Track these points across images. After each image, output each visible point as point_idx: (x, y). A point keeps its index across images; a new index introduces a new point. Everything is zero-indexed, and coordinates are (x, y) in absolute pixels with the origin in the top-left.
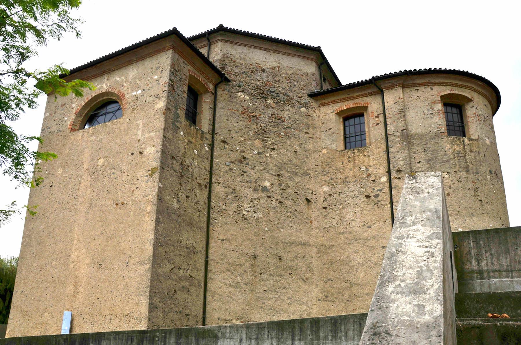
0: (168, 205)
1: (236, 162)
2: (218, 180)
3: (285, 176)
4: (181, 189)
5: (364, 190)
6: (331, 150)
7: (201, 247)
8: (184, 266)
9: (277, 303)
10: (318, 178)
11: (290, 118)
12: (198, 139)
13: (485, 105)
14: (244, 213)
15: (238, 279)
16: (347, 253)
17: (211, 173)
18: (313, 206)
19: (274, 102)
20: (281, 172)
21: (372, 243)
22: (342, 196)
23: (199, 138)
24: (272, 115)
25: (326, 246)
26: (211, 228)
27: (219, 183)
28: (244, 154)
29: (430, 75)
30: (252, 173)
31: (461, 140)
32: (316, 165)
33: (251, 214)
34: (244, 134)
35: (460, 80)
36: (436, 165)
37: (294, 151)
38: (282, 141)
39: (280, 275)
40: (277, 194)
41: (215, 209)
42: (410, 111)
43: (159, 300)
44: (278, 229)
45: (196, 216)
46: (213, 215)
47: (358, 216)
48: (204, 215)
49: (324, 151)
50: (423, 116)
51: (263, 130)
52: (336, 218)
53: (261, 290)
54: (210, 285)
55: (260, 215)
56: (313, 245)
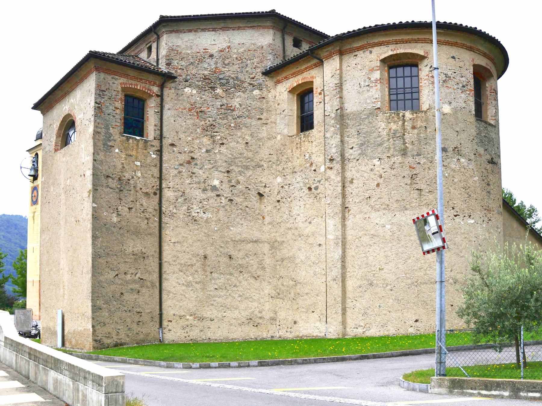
0: (106, 220)
1: (185, 164)
2: (168, 185)
3: (235, 172)
4: (120, 204)
5: (307, 181)
6: (284, 135)
7: (153, 250)
8: (132, 271)
9: (228, 301)
10: (271, 169)
11: (240, 105)
12: (140, 150)
13: (453, 57)
14: (194, 214)
15: (190, 278)
16: (293, 250)
17: (161, 179)
18: (266, 201)
19: (223, 91)
20: (231, 168)
21: (311, 240)
22: (291, 188)
23: (141, 149)
24: (221, 106)
25: (279, 242)
26: (163, 232)
27: (169, 188)
28: (192, 155)
29: (362, 36)
30: (201, 173)
31: (401, 115)
32: (270, 154)
33: (200, 215)
34: (192, 133)
35: (408, 34)
36: (368, 150)
37: (244, 142)
38: (232, 134)
39: (231, 274)
40: (226, 192)
41: (166, 213)
42: (347, 85)
43: (103, 302)
44: (228, 227)
45: (144, 225)
46: (165, 219)
47: (302, 211)
48: (156, 221)
49: (279, 137)
50: (359, 89)
51: (212, 125)
52: (287, 213)
53: (212, 289)
54: (165, 285)
55: (210, 216)
56: (266, 242)
